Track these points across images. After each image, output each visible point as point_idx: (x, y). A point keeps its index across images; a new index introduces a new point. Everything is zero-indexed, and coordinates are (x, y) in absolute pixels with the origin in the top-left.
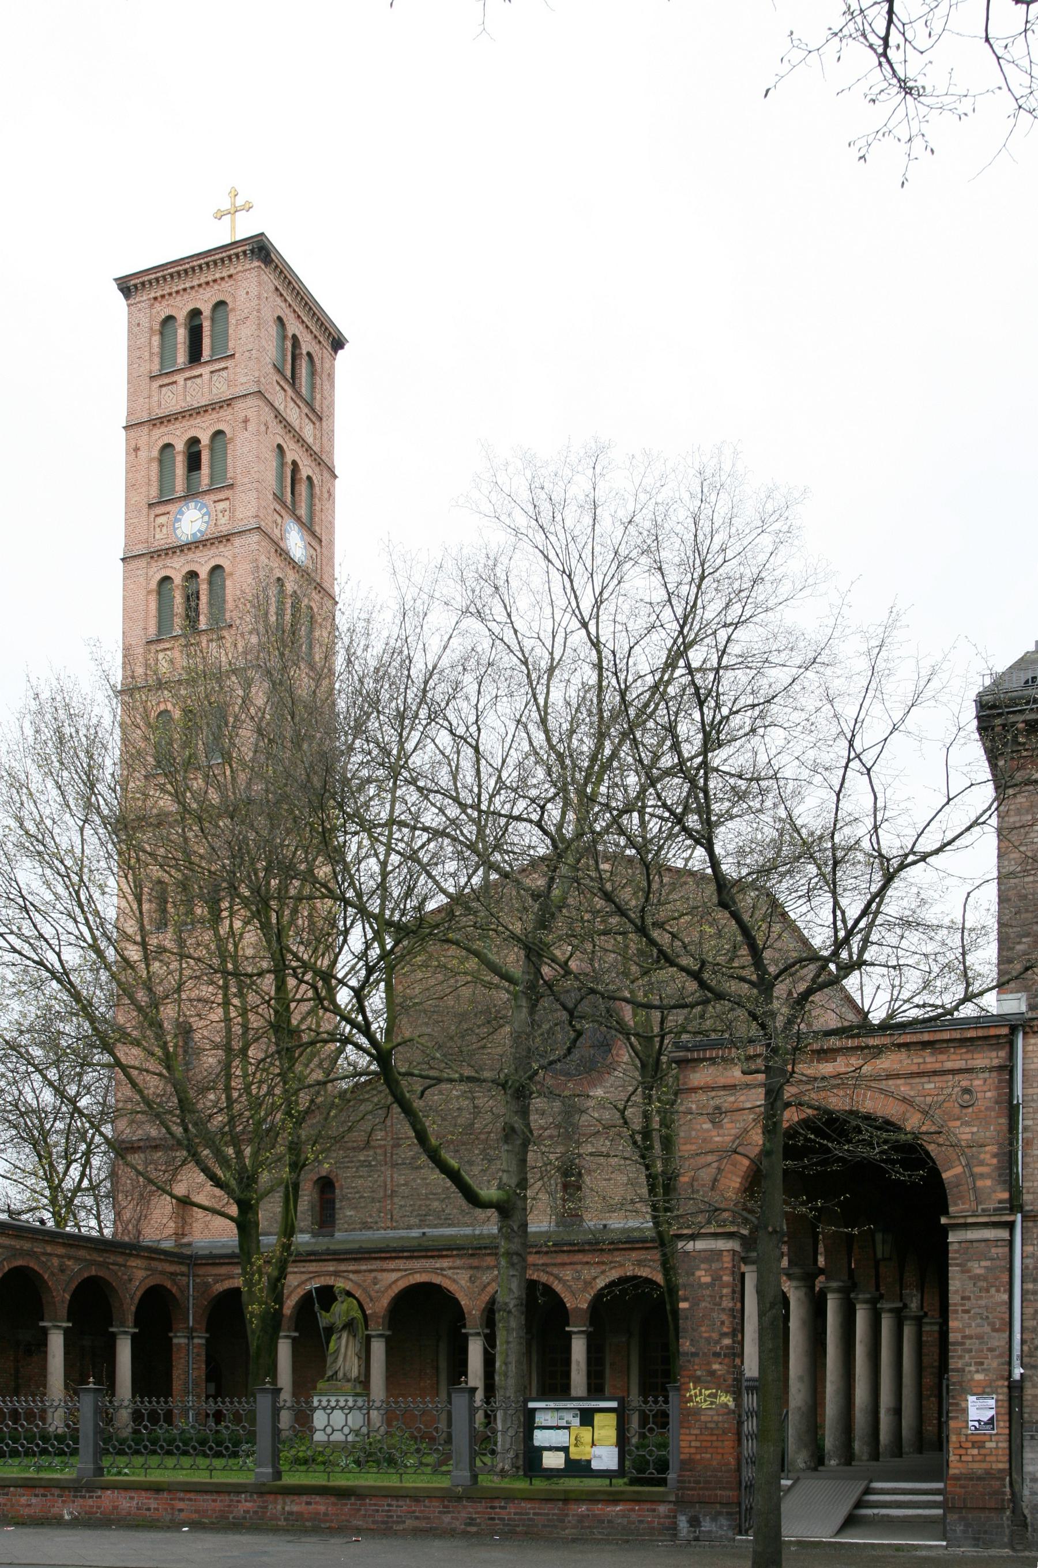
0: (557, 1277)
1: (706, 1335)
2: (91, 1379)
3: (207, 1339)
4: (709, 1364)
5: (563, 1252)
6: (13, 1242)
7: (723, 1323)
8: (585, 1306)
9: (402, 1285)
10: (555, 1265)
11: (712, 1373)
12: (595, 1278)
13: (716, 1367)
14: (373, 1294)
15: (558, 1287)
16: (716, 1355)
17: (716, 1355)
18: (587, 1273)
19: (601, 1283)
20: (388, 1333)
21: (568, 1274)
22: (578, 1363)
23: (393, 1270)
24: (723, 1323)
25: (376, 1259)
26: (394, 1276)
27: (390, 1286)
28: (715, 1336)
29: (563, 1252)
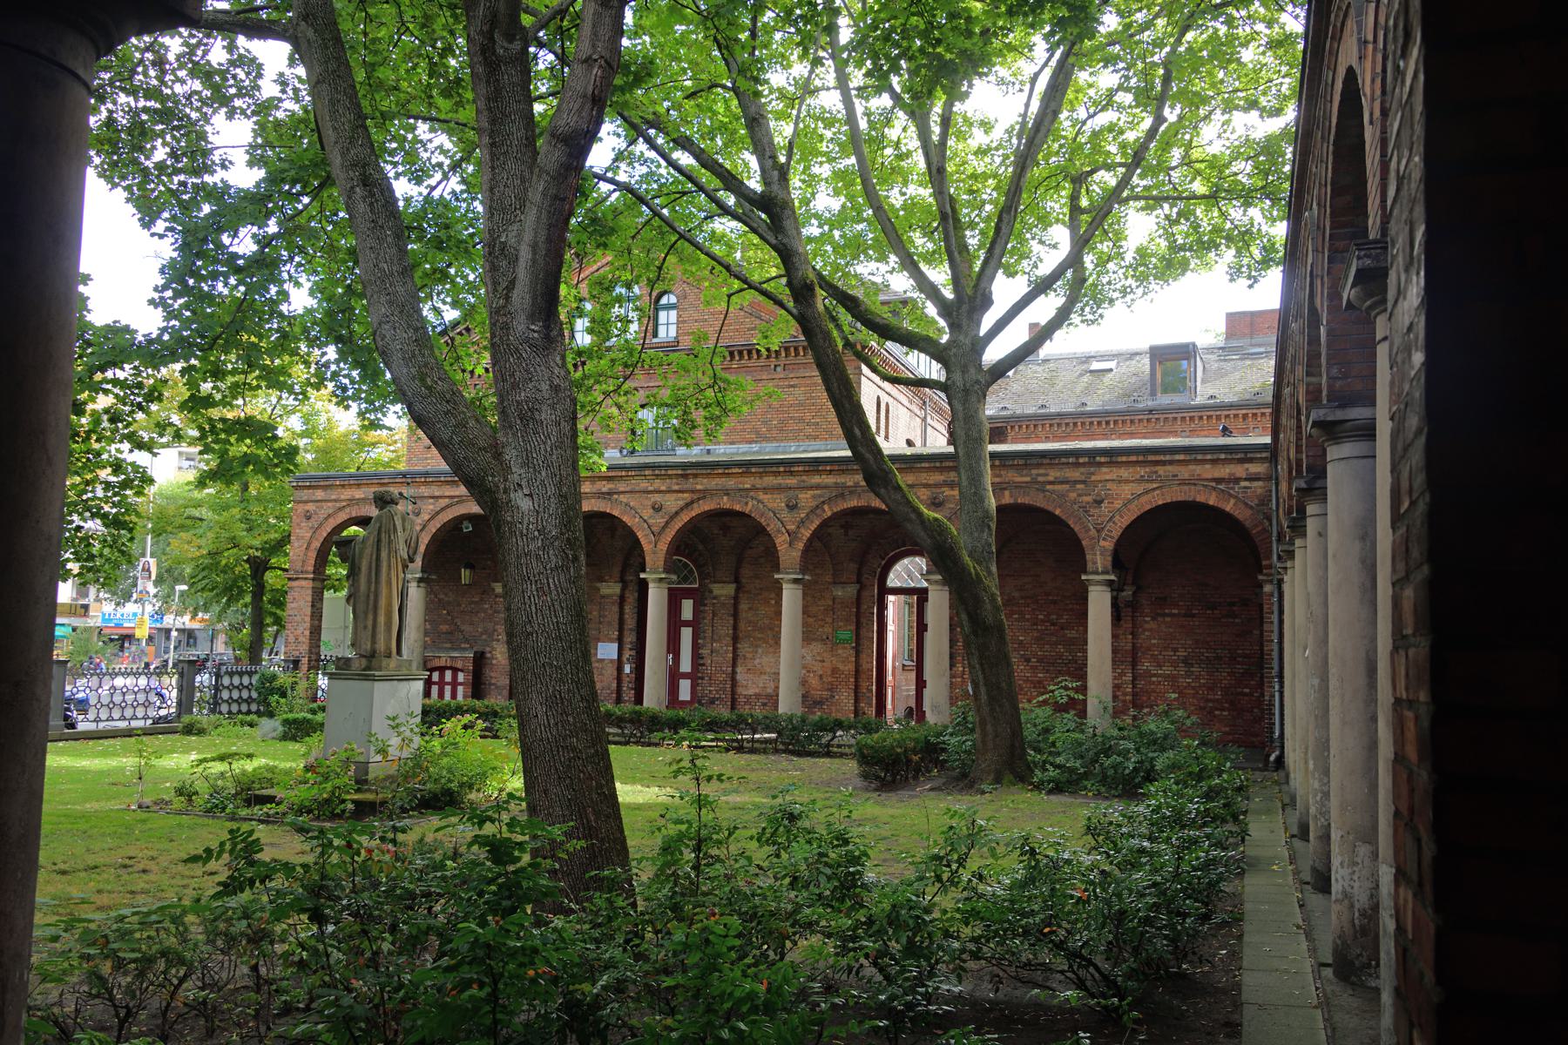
6: (840, 479)
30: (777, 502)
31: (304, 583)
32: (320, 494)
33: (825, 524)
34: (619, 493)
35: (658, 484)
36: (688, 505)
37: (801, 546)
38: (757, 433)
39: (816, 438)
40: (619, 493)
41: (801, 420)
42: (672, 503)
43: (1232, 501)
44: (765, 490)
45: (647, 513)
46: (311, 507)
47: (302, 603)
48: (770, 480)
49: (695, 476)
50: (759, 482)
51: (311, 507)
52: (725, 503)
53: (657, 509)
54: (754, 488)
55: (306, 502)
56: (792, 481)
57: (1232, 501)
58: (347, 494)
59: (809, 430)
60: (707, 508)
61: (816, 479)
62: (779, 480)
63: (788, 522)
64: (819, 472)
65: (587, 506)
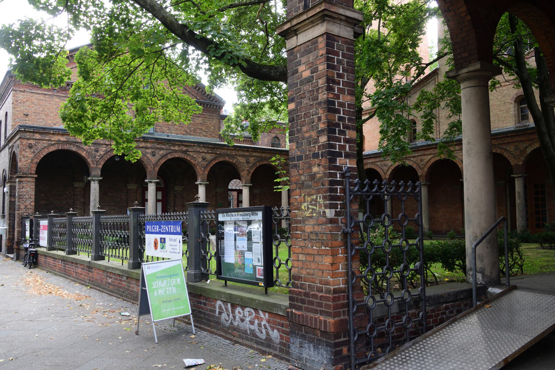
0: (505, 150)
1: (307, 135)
2: (71, 209)
3: (36, 178)
4: (310, 168)
5: (508, 137)
6: (261, 155)
7: (319, 119)
8: (521, 163)
9: (433, 161)
10: (505, 144)
11: (313, 177)
12: (526, 148)
13: (315, 169)
14: (421, 166)
15: (506, 155)
16: (316, 156)
17: (316, 156)
18: (522, 146)
19: (529, 151)
20: (428, 183)
21: (511, 148)
22: (519, 193)
23: (429, 155)
24: (319, 119)
25: (421, 150)
26: (429, 157)
27: (428, 162)
28: (314, 134)
29: (508, 137)
30: (242, 160)
31: (29, 179)
32: (37, 136)
33: (257, 168)
34: (190, 151)
35: (203, 150)
36: (215, 159)
37: (250, 175)
38: (186, 132)
39: (206, 136)
40: (190, 151)
41: (201, 129)
42: (209, 157)
43: (85, 152)
44: (240, 156)
45: (200, 160)
46: (32, 142)
47: (29, 189)
48: (240, 153)
49: (217, 148)
50: (237, 153)
51: (32, 142)
52: (227, 159)
53: (204, 159)
54: (236, 155)
55: (29, 139)
56: (247, 154)
57: (85, 152)
58: (56, 138)
59: (204, 133)
60: (221, 160)
61: (254, 154)
62: (243, 153)
63: (201, 162)
64: (255, 152)
65: (366, 167)
